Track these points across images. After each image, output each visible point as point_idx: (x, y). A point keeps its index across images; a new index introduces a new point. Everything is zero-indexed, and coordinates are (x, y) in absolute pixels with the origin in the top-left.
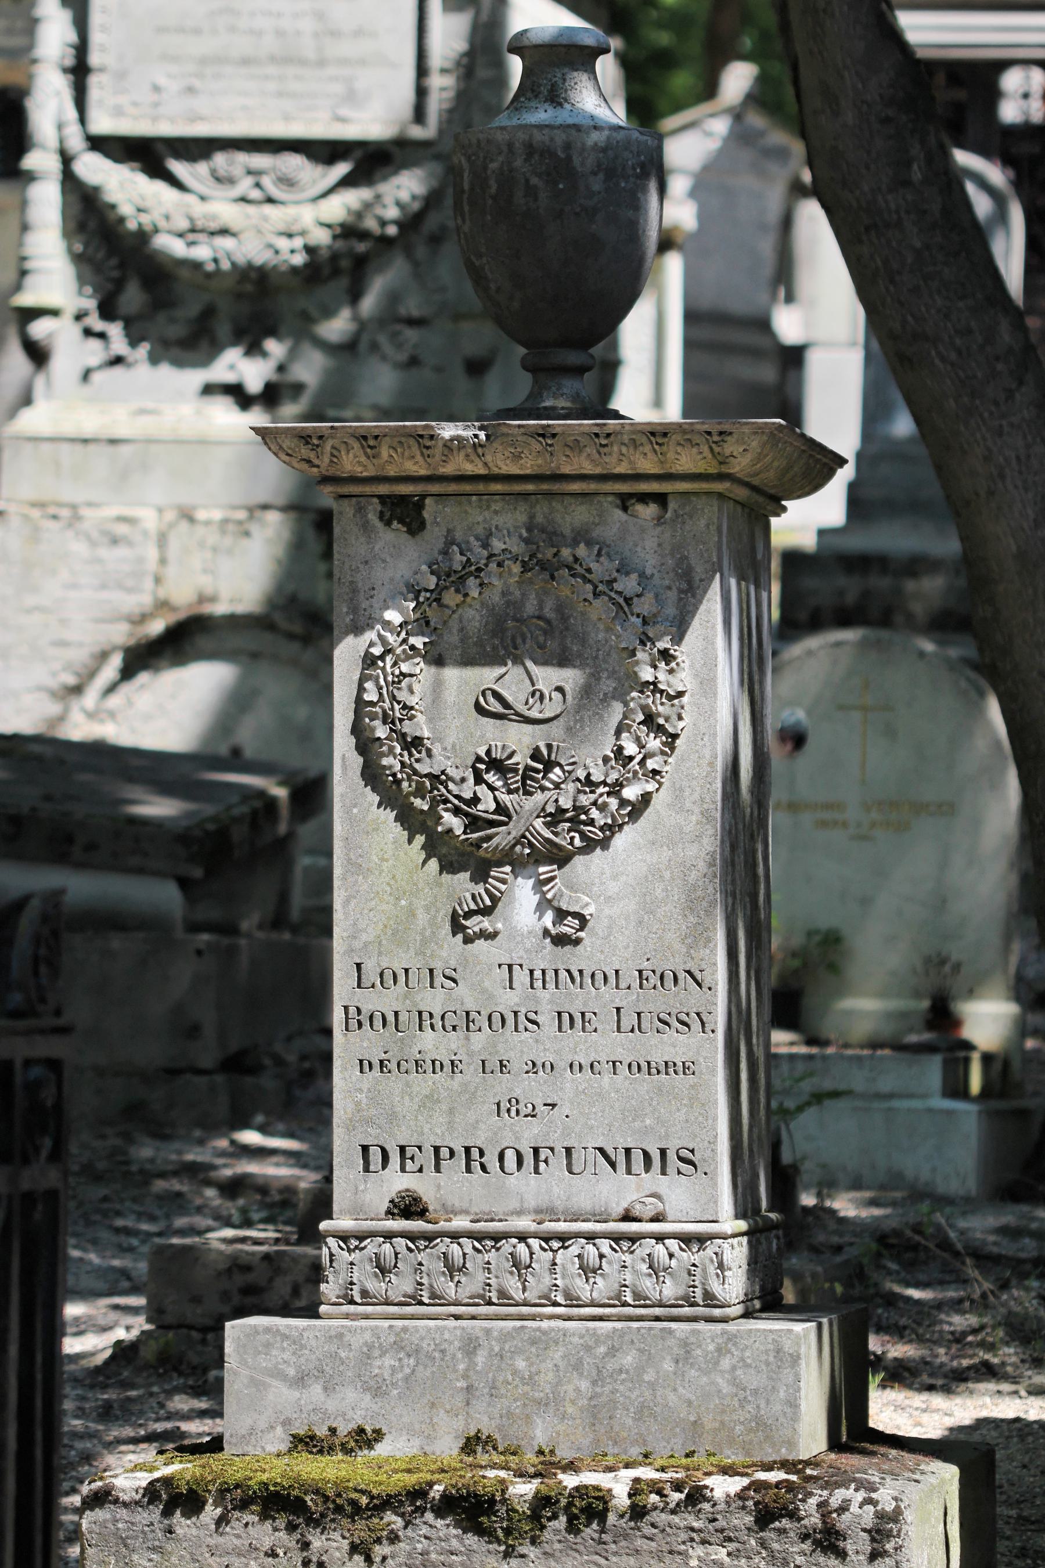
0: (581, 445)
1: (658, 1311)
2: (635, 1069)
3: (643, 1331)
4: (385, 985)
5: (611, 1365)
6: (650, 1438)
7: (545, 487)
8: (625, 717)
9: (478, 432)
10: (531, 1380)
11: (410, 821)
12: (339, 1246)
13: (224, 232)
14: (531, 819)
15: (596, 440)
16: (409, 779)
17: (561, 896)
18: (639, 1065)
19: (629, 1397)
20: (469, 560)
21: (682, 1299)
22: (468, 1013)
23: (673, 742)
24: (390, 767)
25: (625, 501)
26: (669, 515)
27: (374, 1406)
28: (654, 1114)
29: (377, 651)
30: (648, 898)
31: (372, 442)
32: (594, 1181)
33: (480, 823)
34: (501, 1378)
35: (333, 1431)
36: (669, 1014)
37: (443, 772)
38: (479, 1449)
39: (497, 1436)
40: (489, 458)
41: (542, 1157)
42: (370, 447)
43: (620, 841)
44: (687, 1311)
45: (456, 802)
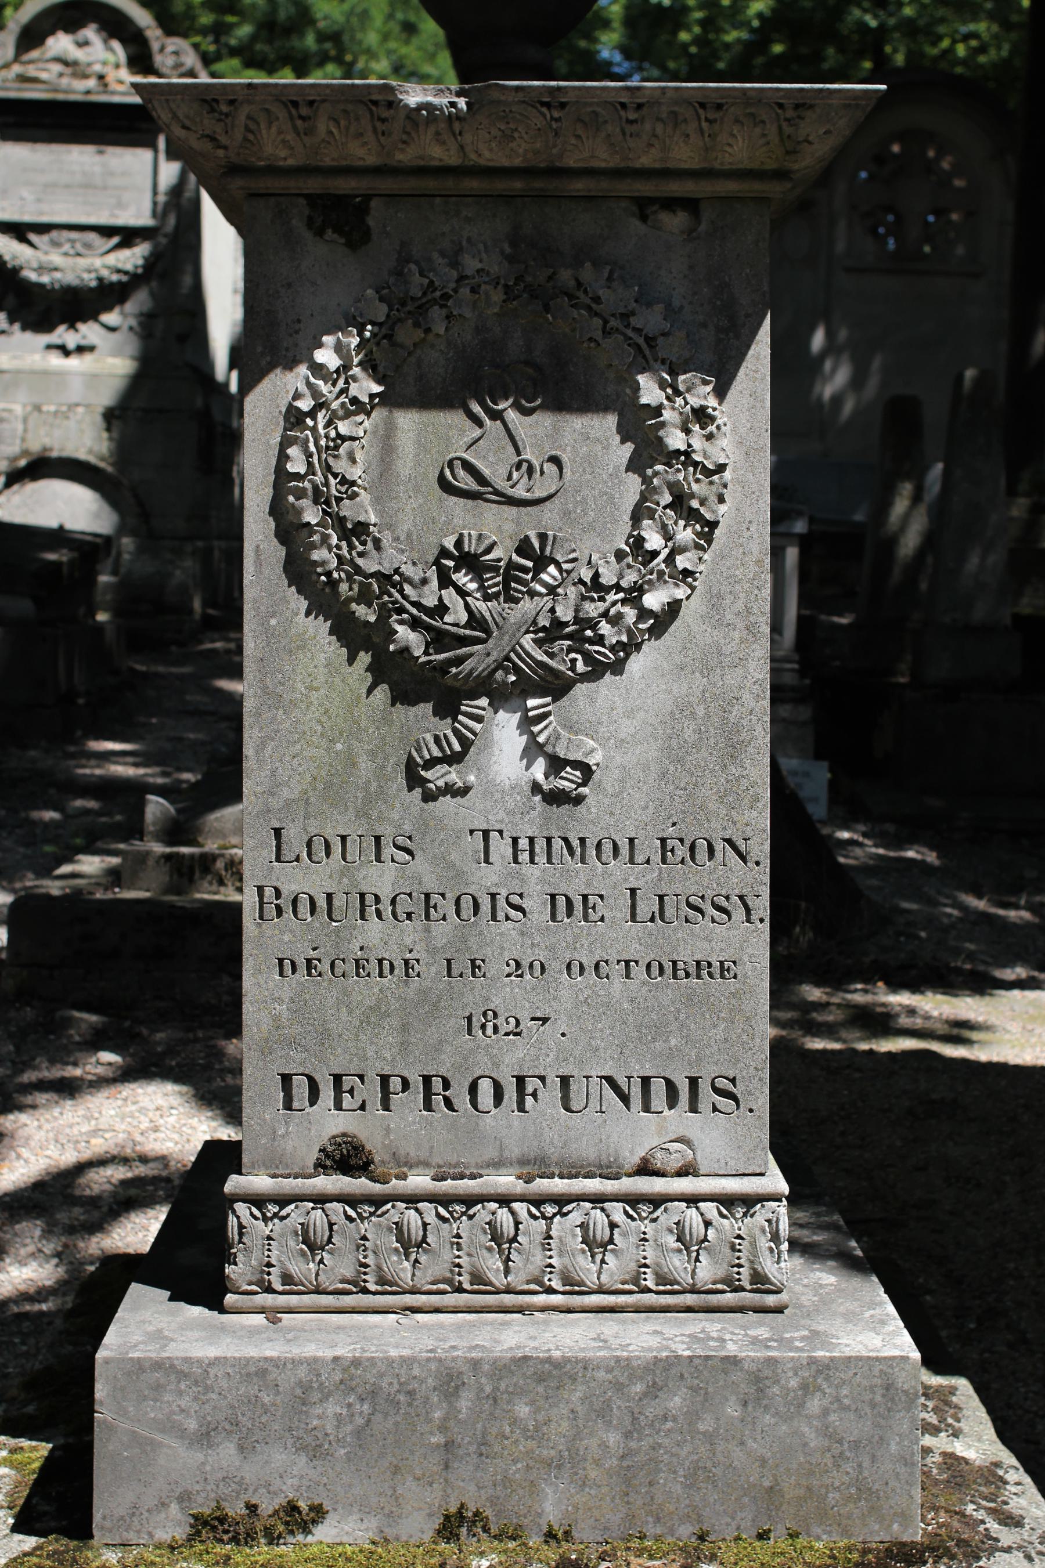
0: (601, 120)
1: (689, 1299)
2: (655, 970)
3: (697, 1361)
4: (315, 858)
5: (651, 1410)
6: (706, 1512)
7: (538, 184)
8: (644, 498)
9: (456, 99)
10: (537, 1433)
11: (350, 634)
12: (252, 1214)
13: (56, 269)
14: (518, 636)
15: (623, 113)
16: (350, 579)
17: (558, 738)
18: (660, 965)
19: (677, 1455)
20: (432, 282)
21: (722, 1281)
22: (427, 896)
23: (712, 532)
24: (323, 563)
25: (643, 207)
26: (703, 227)
27: (311, 1472)
28: (681, 1031)
29: (305, 404)
30: (674, 742)
31: (304, 111)
32: (599, 1121)
33: (446, 640)
34: (494, 1431)
35: (252, 1508)
36: (702, 897)
37: (397, 571)
38: (464, 1530)
39: (488, 1512)
40: (467, 138)
41: (530, 1089)
42: (301, 117)
43: (636, 664)
44: (729, 1298)
45: (414, 611)
